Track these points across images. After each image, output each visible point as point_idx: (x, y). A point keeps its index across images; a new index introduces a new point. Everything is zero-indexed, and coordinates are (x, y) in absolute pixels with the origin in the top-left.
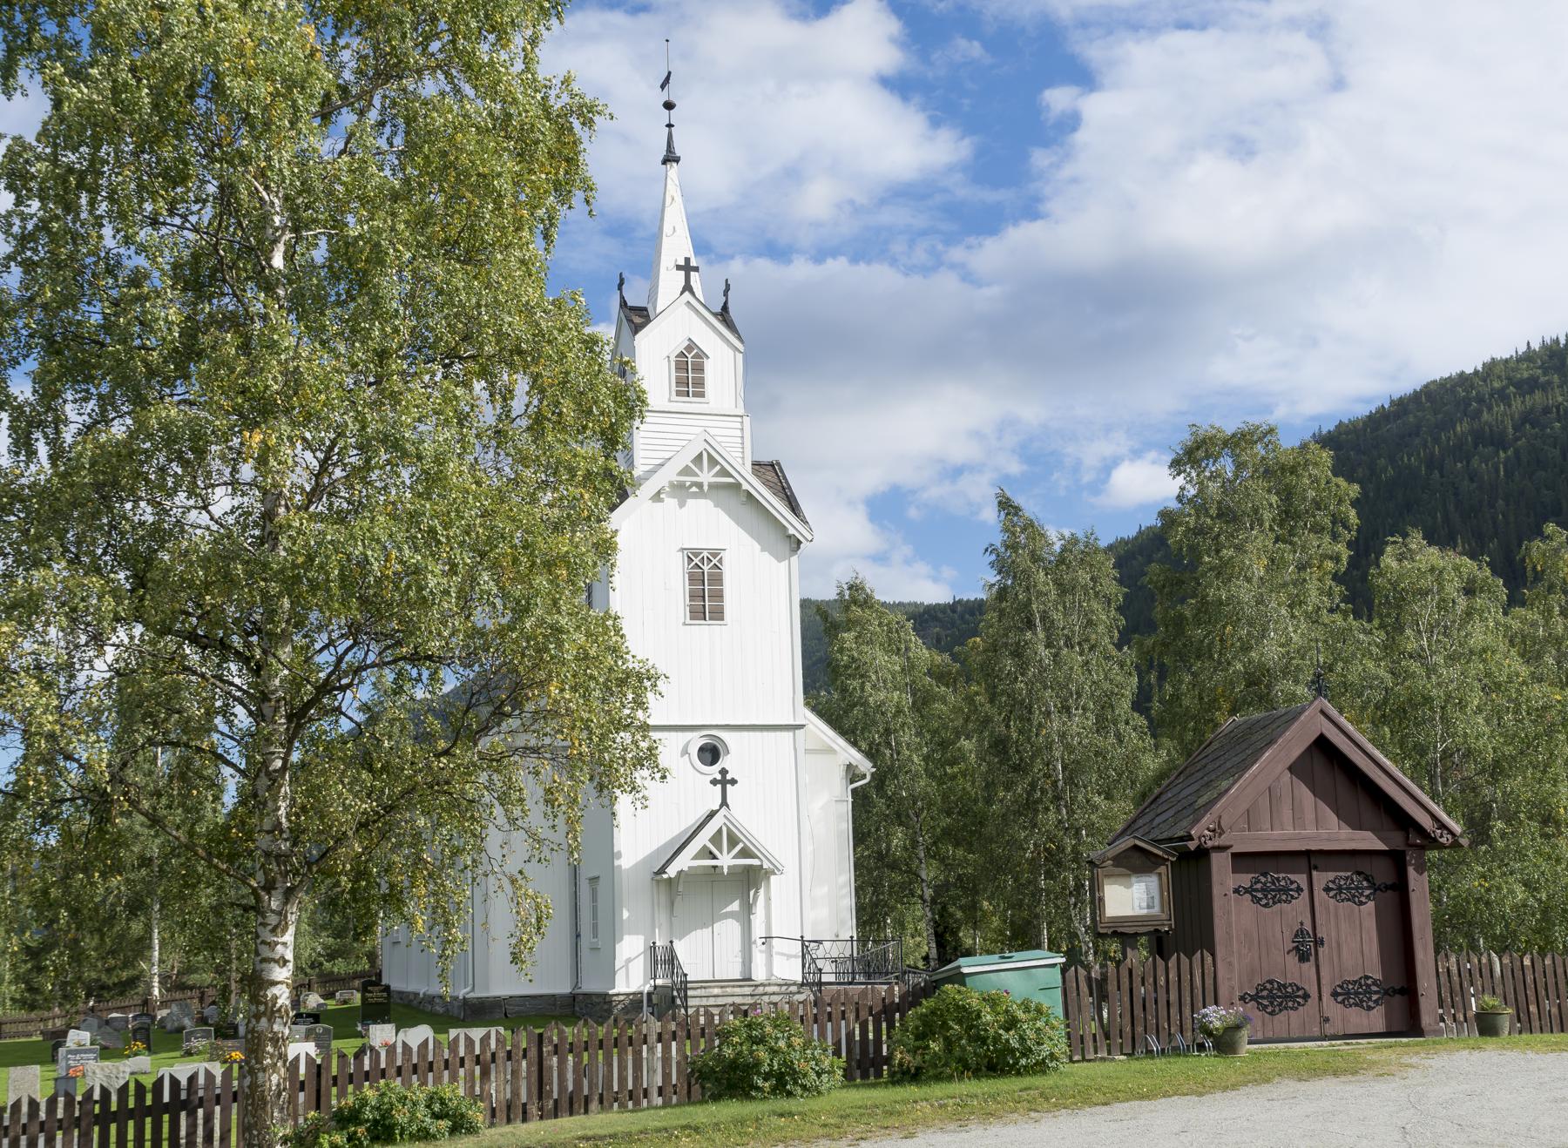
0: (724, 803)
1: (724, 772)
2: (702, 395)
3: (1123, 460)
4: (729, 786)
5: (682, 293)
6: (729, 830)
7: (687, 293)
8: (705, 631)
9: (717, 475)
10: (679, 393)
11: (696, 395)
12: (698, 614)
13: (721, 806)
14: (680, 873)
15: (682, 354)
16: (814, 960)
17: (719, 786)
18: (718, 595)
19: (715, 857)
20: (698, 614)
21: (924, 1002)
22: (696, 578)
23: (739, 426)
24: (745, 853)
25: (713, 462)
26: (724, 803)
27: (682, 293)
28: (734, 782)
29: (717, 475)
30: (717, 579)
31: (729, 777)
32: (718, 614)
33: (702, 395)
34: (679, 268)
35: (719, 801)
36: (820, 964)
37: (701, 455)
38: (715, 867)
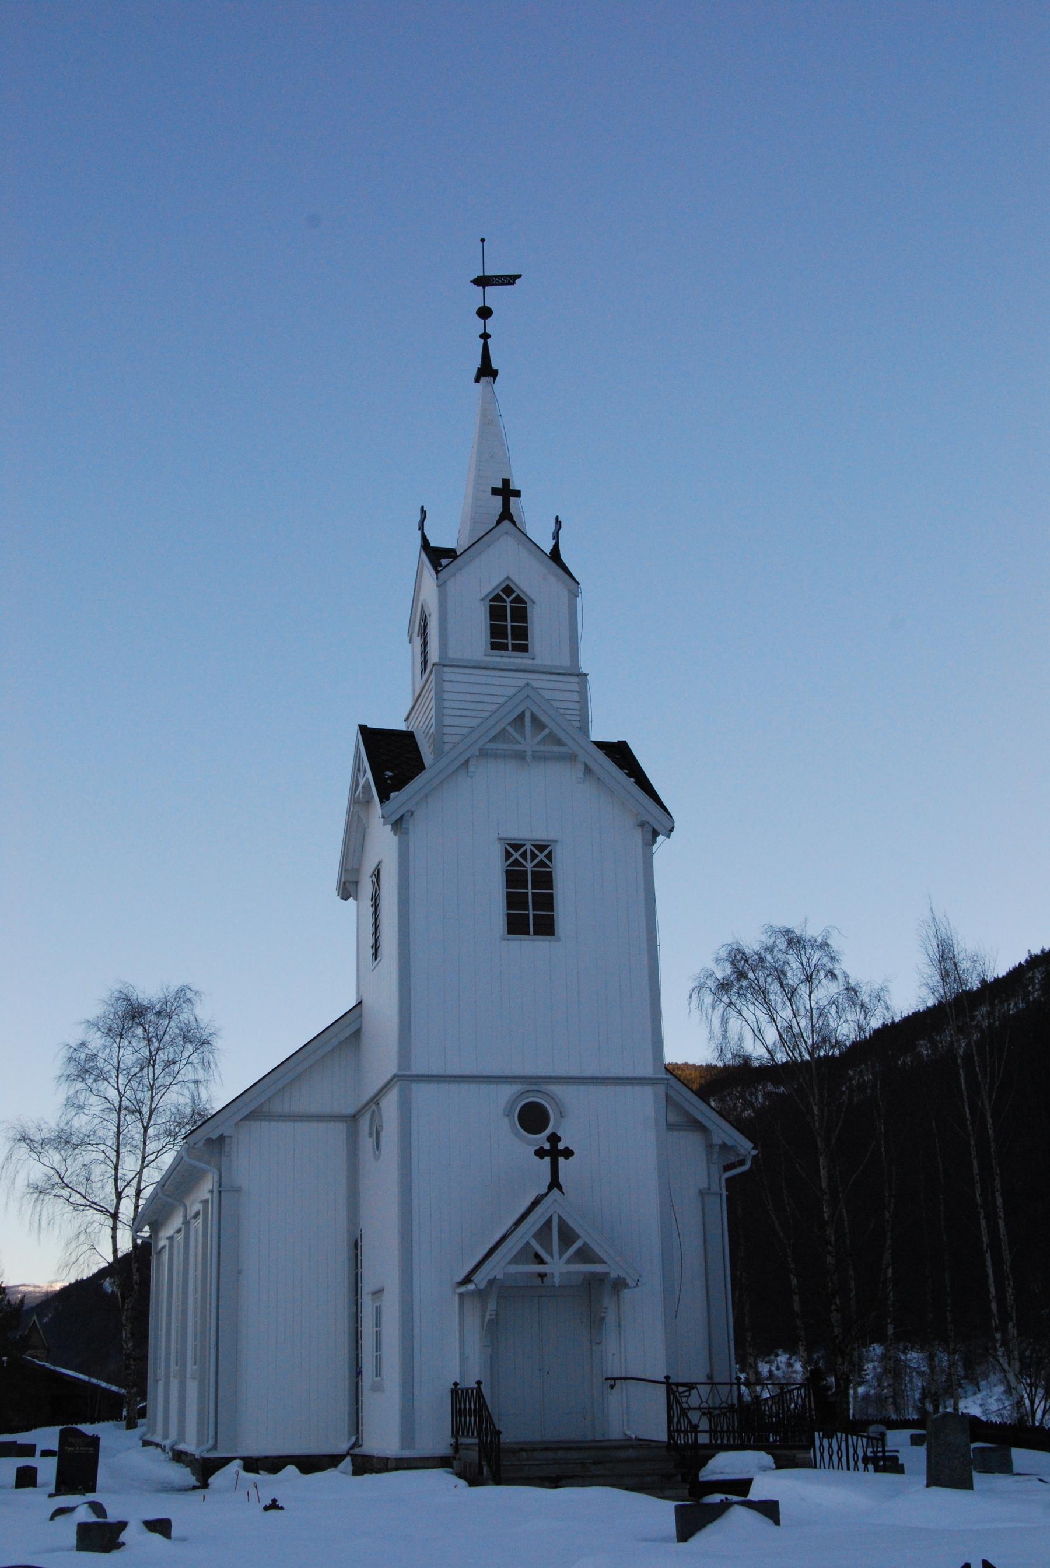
0: (555, 1183)
1: (554, 1139)
2: (525, 648)
3: (673, 1070)
4: (561, 1160)
5: (499, 522)
6: (508, 844)
7: (556, 1190)
8: (532, 946)
9: (543, 741)
10: (494, 646)
11: (517, 648)
12: (516, 926)
13: (550, 1188)
14: (491, 1282)
15: (497, 598)
16: (684, 1412)
17: (547, 1159)
18: (546, 902)
19: (541, 1261)
20: (516, 926)
21: (738, 1366)
22: (514, 878)
23: (576, 688)
24: (585, 1255)
25: (538, 724)
26: (555, 1183)
27: (499, 522)
28: (568, 1153)
29: (543, 741)
30: (545, 879)
31: (561, 1146)
32: (546, 927)
33: (525, 648)
34: (495, 491)
35: (547, 1180)
36: (694, 1417)
37: (522, 716)
38: (542, 1276)
